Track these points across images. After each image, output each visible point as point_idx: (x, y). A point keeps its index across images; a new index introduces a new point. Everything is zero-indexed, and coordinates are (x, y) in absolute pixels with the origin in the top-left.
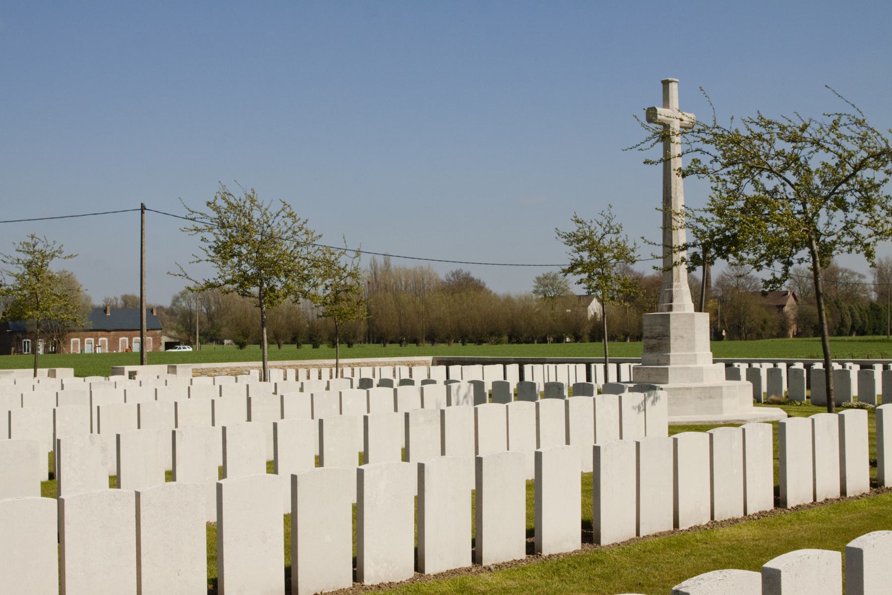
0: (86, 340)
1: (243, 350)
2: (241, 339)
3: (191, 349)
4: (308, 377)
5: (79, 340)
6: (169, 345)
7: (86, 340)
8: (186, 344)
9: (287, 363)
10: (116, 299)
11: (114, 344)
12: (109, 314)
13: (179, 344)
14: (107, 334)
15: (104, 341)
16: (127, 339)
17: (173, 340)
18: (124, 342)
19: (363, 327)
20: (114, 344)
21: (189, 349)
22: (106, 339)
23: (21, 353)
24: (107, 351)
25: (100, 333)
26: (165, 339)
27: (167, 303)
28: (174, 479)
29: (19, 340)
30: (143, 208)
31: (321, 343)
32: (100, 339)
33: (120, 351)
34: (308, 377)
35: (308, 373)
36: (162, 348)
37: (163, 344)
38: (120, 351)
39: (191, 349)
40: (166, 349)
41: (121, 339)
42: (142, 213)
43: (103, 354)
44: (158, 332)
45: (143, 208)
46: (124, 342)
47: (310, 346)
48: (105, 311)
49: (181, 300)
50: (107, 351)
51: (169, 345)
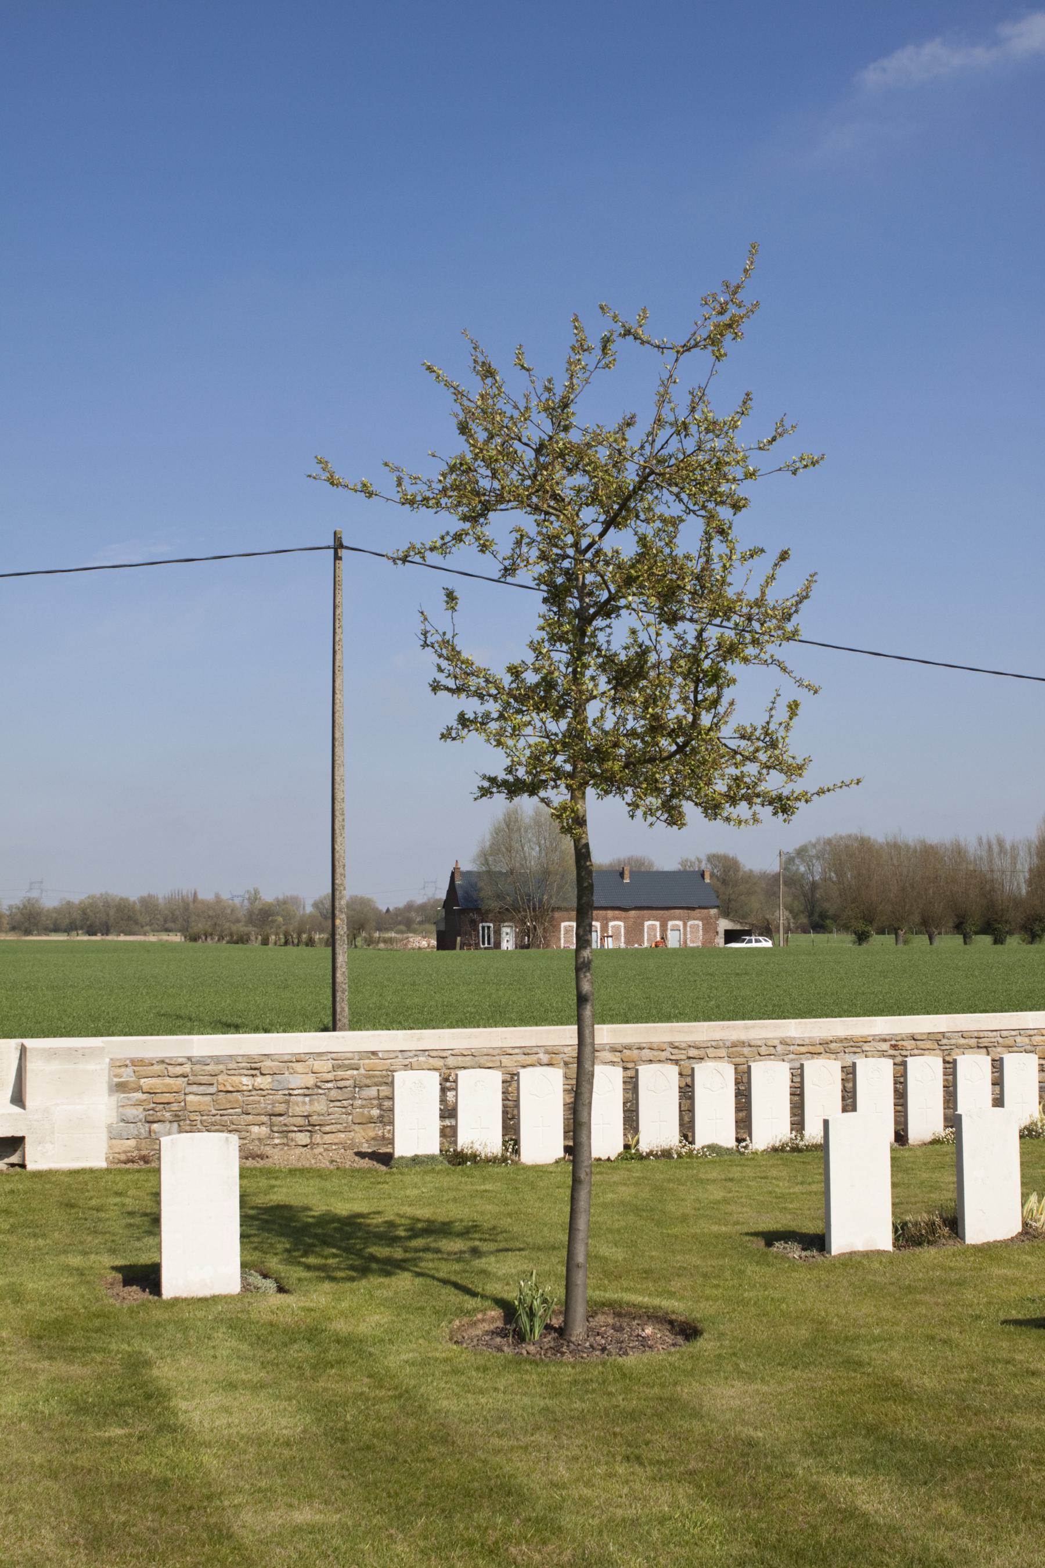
0: (670, 923)
1: (864, 945)
2: (860, 926)
3: (769, 944)
4: (849, 1102)
5: (657, 923)
6: (731, 936)
7: (670, 923)
8: (761, 935)
9: (795, 1028)
10: (700, 861)
11: (634, 932)
12: (627, 881)
13: (749, 933)
14: (623, 914)
15: (618, 928)
16: (657, 923)
17: (738, 927)
18: (652, 928)
19: (52, 926)
20: (634, 932)
21: (767, 944)
22: (621, 924)
23: (477, 947)
24: (623, 946)
25: (610, 913)
26: (724, 924)
27: (773, 866)
28: (854, 1109)
29: (474, 924)
30: (338, 545)
31: (1010, 933)
32: (611, 924)
33: (646, 945)
34: (849, 1102)
35: (850, 1074)
36: (720, 941)
37: (722, 934)
38: (646, 945)
39: (769, 944)
40: (727, 942)
41: (647, 924)
42: (337, 557)
43: (617, 951)
44: (713, 912)
45: (338, 545)
46: (652, 928)
47: (987, 939)
48: (622, 875)
49: (797, 861)
50: (623, 946)
51: (731, 936)
